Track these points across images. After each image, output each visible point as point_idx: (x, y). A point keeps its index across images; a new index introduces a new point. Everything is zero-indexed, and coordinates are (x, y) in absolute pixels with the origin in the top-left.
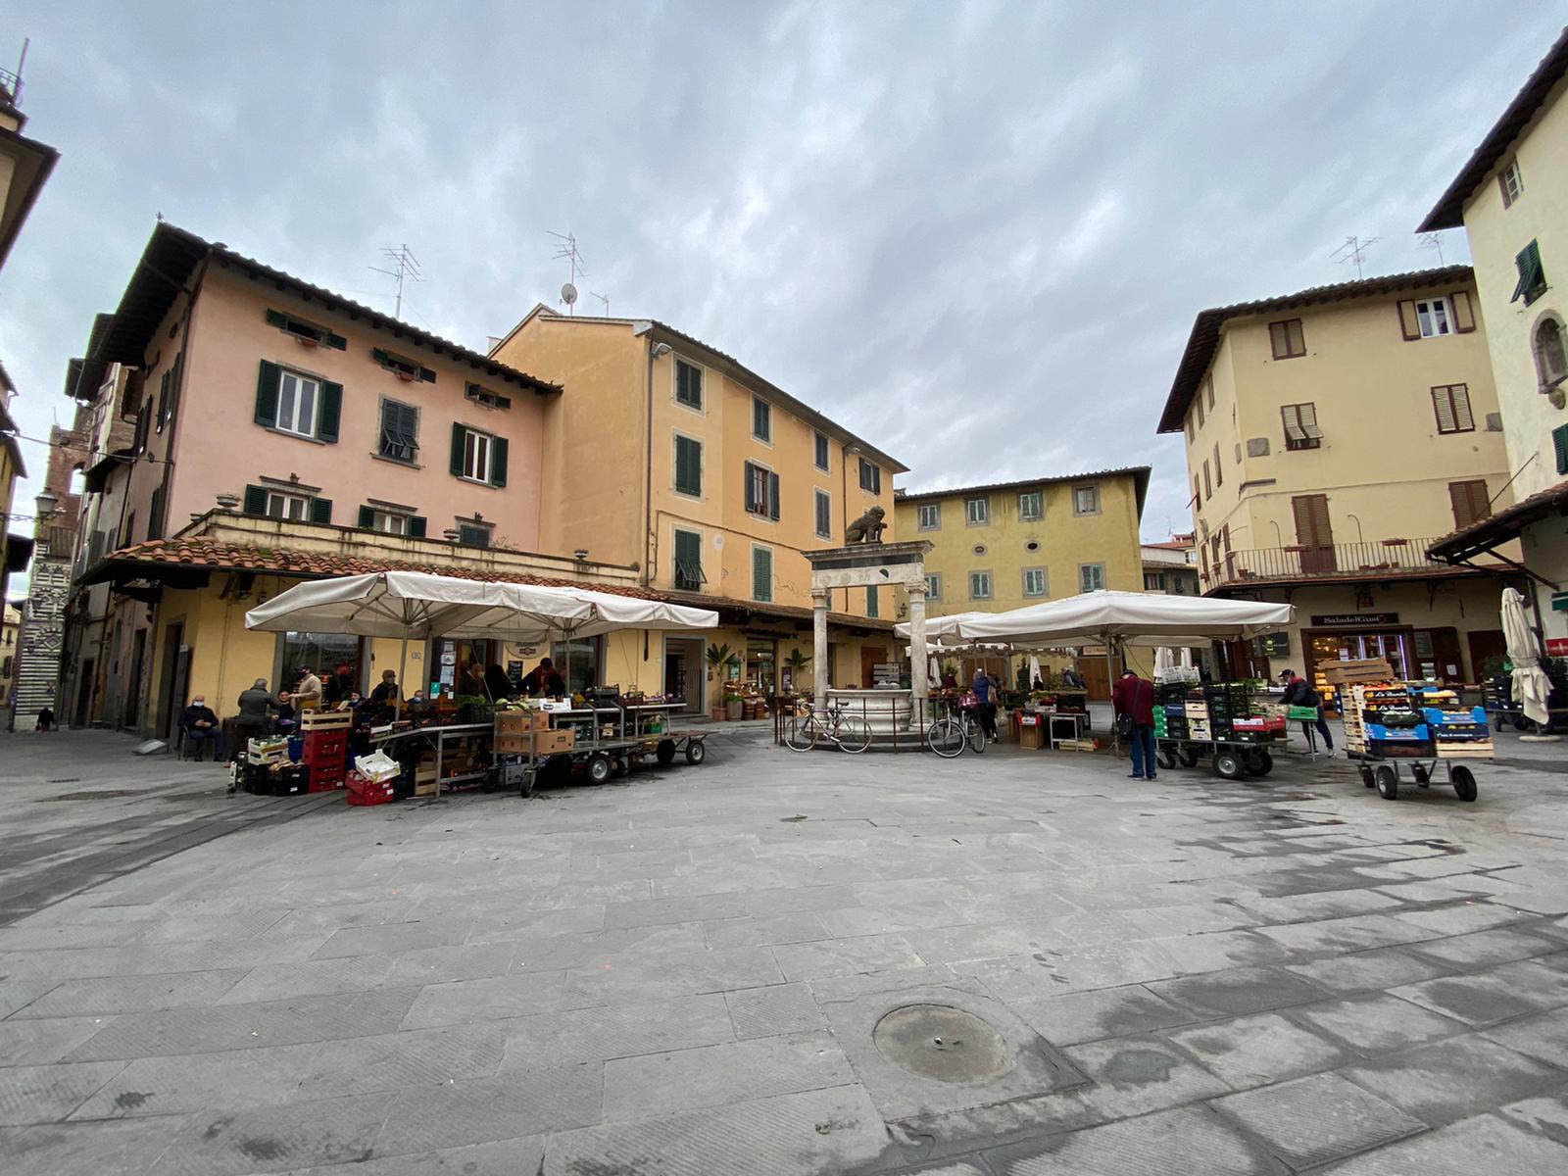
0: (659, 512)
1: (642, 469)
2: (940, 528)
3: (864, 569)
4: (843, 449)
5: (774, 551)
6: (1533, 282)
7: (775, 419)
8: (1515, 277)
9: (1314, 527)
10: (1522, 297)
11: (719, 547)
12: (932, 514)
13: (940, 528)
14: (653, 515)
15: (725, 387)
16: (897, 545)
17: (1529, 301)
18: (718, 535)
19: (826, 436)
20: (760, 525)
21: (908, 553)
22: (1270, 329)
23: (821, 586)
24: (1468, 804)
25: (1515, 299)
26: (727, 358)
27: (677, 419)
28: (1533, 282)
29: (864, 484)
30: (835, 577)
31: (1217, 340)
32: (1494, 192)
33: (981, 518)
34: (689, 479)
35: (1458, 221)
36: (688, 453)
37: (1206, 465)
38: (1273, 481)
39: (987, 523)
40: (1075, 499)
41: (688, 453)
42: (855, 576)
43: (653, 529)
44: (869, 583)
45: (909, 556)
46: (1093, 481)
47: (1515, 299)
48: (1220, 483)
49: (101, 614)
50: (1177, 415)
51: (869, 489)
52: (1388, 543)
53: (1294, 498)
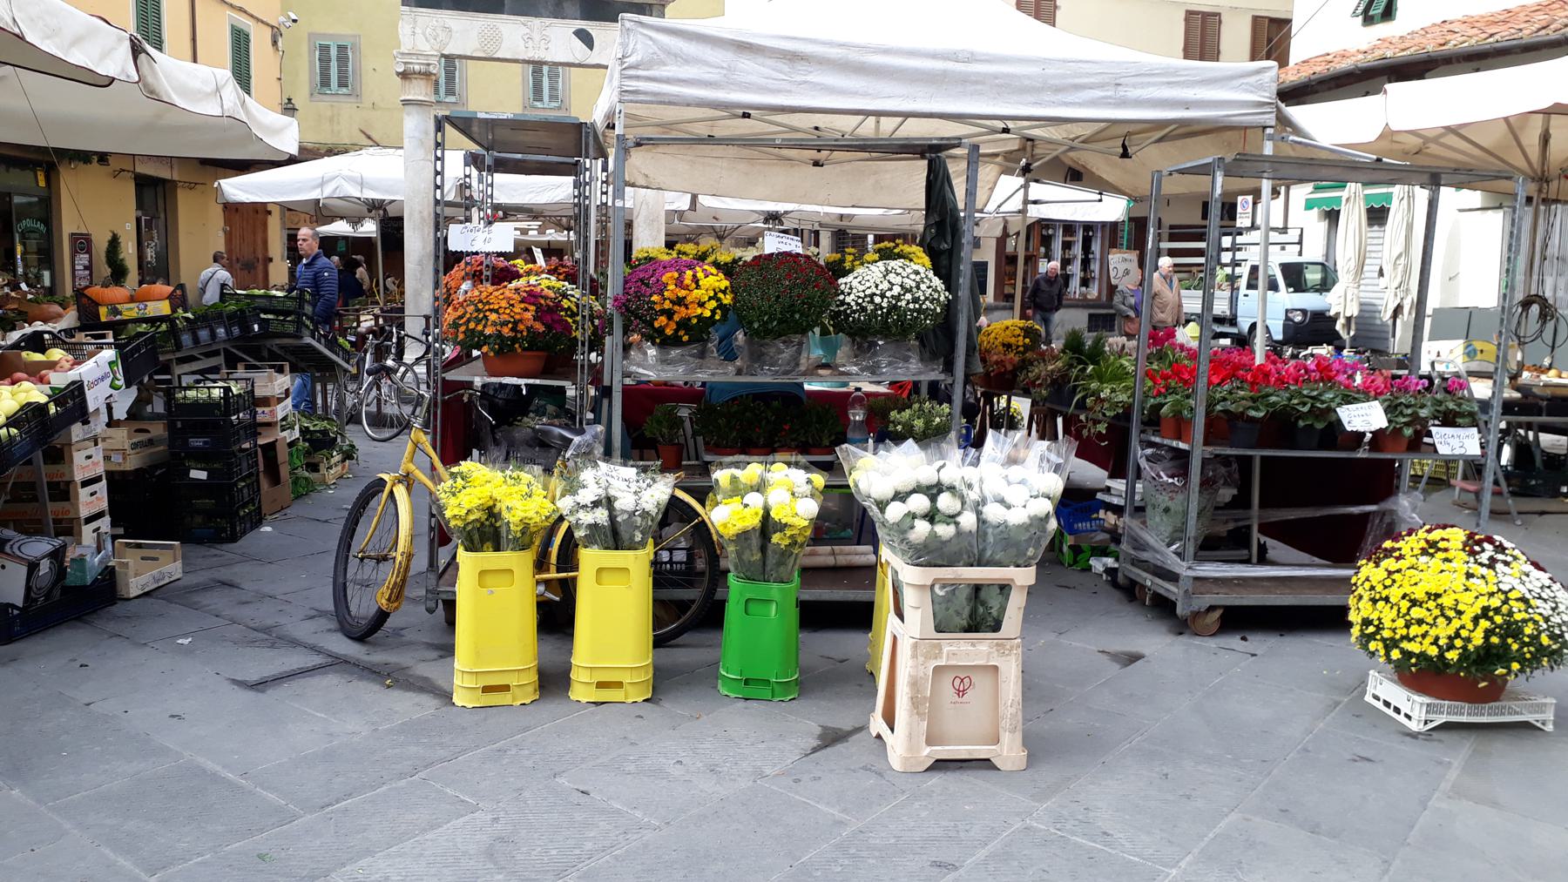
3: (536, 22)
23: (425, 47)
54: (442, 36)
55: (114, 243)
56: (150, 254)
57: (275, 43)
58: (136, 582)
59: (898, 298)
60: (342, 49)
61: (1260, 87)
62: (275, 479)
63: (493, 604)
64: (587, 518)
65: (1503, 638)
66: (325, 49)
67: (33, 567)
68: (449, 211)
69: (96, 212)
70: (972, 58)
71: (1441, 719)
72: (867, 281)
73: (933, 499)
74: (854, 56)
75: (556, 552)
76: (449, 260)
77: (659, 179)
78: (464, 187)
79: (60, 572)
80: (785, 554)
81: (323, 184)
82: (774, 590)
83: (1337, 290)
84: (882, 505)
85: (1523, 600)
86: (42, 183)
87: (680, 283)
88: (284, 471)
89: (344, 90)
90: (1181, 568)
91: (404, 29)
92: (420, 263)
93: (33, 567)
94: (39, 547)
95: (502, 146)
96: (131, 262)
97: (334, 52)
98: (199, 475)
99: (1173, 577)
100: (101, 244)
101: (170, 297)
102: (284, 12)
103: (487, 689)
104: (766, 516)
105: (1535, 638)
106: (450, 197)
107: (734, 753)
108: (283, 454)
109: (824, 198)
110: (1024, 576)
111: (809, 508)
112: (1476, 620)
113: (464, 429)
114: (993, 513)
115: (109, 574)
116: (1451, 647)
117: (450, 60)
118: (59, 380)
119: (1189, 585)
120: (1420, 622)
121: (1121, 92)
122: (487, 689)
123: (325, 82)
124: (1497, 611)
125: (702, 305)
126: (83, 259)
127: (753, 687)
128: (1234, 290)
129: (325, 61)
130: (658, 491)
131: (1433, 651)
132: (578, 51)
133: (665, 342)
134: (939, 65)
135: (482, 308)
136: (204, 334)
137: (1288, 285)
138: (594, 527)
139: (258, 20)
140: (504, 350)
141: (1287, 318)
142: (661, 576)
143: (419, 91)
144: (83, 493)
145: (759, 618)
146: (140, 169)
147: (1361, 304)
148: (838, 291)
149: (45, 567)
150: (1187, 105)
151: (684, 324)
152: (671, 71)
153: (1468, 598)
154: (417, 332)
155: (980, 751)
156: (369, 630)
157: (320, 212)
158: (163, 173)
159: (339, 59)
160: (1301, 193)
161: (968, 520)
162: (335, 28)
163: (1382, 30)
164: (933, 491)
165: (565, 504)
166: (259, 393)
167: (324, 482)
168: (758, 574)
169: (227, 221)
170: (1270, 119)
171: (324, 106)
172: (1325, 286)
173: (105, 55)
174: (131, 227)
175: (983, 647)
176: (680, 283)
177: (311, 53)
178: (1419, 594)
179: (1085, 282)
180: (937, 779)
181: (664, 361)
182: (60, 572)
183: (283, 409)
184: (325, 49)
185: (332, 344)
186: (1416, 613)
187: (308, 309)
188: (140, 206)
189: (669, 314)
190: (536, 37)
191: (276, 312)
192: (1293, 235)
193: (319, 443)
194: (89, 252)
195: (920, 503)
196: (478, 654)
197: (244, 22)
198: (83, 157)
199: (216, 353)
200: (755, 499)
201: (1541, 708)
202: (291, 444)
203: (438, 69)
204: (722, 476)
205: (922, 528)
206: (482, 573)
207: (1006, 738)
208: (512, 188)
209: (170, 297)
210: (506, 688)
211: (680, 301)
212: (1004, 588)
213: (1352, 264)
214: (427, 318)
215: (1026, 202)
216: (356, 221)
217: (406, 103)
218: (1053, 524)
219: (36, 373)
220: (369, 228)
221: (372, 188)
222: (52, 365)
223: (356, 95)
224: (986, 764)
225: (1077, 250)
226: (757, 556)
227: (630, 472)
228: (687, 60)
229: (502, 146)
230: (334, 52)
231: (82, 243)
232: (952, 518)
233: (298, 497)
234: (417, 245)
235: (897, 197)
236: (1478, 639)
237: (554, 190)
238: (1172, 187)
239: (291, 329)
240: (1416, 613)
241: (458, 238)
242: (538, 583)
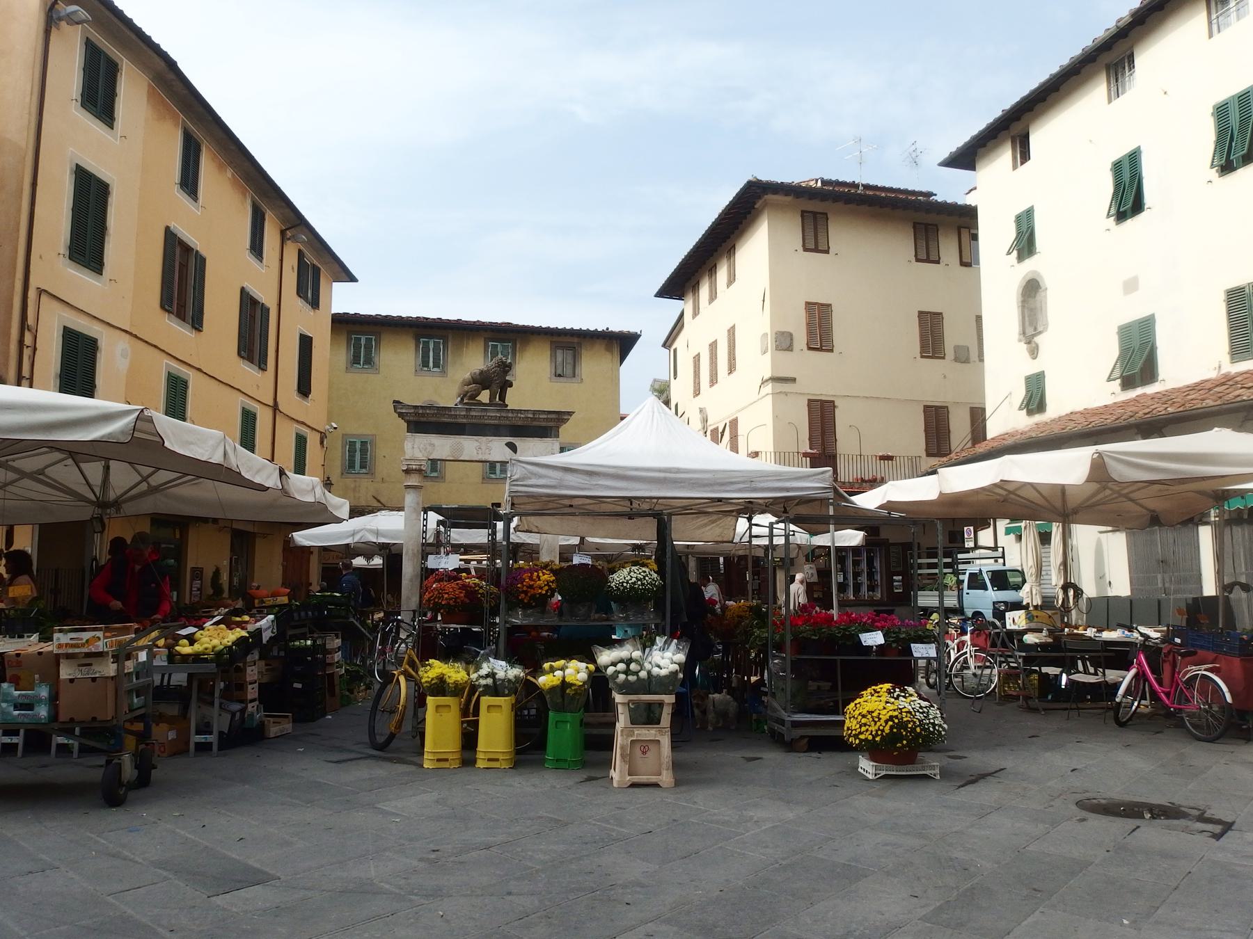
0: (41, 292)
1: (19, 210)
2: (377, 371)
3: (484, 439)
4: (283, 233)
5: (193, 378)
6: (1025, 244)
7: (209, 170)
8: (1012, 235)
9: (823, 433)
10: (1015, 252)
11: (122, 365)
12: (368, 348)
13: (377, 371)
14: (32, 294)
15: (151, 94)
16: (535, 412)
17: (1020, 258)
18: (124, 343)
19: (264, 207)
20: (173, 331)
21: (544, 424)
22: (802, 216)
23: (420, 455)
24: (469, 769)
25: (1009, 253)
26: (164, 56)
27: (76, 139)
28: (1025, 244)
29: (301, 292)
30: (441, 446)
31: (750, 213)
32: (1005, 156)
33: (436, 365)
34: (88, 246)
35: (971, 167)
36: (91, 195)
37: (713, 346)
38: (794, 380)
39: (444, 372)
40: (553, 357)
41: (91, 195)
42: (471, 447)
43: (31, 320)
44: (491, 459)
45: (545, 428)
46: (576, 340)
47: (1009, 253)
48: (732, 368)
49: (153, 484)
50: (682, 283)
51: (305, 298)
52: (883, 458)
53: (809, 401)
54: (429, 448)
55: (217, 573)
56: (236, 580)
57: (322, 443)
58: (274, 730)
59: (634, 583)
60: (364, 444)
61: (824, 480)
62: (333, 694)
63: (440, 725)
64: (483, 682)
65: (899, 730)
66: (352, 444)
67: (233, 715)
68: (428, 549)
69: (207, 555)
70: (678, 471)
71: (883, 773)
72: (623, 577)
73: (628, 666)
74: (621, 472)
75: (469, 701)
76: (427, 573)
77: (548, 529)
78: (438, 533)
79: (242, 719)
80: (573, 698)
81: (354, 534)
82: (568, 716)
83: (1026, 587)
84: (606, 667)
85: (909, 712)
86: (178, 536)
87: (531, 578)
88: (337, 689)
90: (784, 715)
91: (408, 446)
92: (411, 580)
93: (233, 715)
94: (236, 707)
95: (457, 517)
96: (226, 587)
97: (358, 446)
98: (298, 686)
99: (782, 722)
100: (208, 574)
101: (288, 595)
102: (329, 421)
103: (439, 760)
104: (564, 681)
105: (913, 730)
106: (431, 541)
107: (545, 789)
108: (337, 681)
109: (607, 539)
110: (669, 699)
111: (583, 676)
112: (886, 722)
113: (429, 647)
114: (656, 671)
115: (262, 724)
116: (877, 735)
117: (434, 462)
118: (251, 628)
119: (788, 725)
120: (865, 725)
121: (754, 485)
122: (439, 760)
123: (352, 465)
124: (896, 717)
125: (541, 588)
126: (197, 583)
127: (561, 765)
128: (960, 590)
129: (352, 451)
130: (515, 672)
131: (870, 737)
132: (506, 454)
133: (525, 607)
134: (662, 475)
135: (441, 591)
136: (303, 614)
137: (993, 586)
138: (486, 686)
139: (313, 429)
140: (451, 613)
141: (995, 608)
142: (517, 709)
143: (414, 480)
144: (250, 687)
145: (563, 731)
146: (234, 526)
147: (1043, 597)
148: (607, 581)
149: (238, 714)
150: (788, 490)
151: (533, 597)
152: (529, 482)
153: (884, 712)
154: (408, 620)
155: (653, 779)
156: (382, 747)
157: (349, 551)
158: (250, 528)
160: (1002, 524)
161: (643, 674)
163: (1038, 418)
164: (628, 661)
165: (474, 676)
166: (328, 647)
167: (356, 699)
168: (561, 709)
169: (285, 559)
170: (831, 495)
171: (349, 481)
172: (1018, 587)
173: (268, 477)
174: (226, 563)
175: (653, 732)
176: (531, 578)
177: (343, 447)
178: (865, 712)
179: (871, 588)
180: (631, 790)
181: (525, 615)
182: (242, 719)
183: (338, 656)
185: (364, 624)
186: (864, 721)
187: (353, 603)
188: (232, 550)
189: (526, 593)
190: (483, 448)
191: (336, 605)
192: (999, 553)
193: (354, 678)
194: (201, 579)
195: (621, 666)
196: (435, 744)
197: (304, 430)
198: (205, 520)
199: (304, 626)
200: (559, 673)
201: (933, 768)
202: (341, 676)
204: (546, 666)
205: (622, 677)
206: (438, 707)
207: (664, 773)
208: (460, 536)
209: (288, 595)
210: (446, 760)
211: (531, 587)
212: (661, 704)
213: (1034, 570)
214: (414, 611)
215: (751, 536)
216: (369, 557)
217: (408, 487)
218: (681, 676)
219: (241, 625)
220: (377, 561)
222: (247, 622)
223: (371, 473)
224: (656, 785)
225: (864, 566)
226: (560, 700)
227: (503, 663)
228: (541, 476)
229: (457, 517)
230: (358, 446)
231: (198, 573)
232: (636, 673)
233: (343, 706)
234: (409, 569)
235: (643, 535)
236: (887, 730)
237: (479, 536)
239: (343, 613)
240: (864, 721)
241: (432, 562)
242: (463, 722)
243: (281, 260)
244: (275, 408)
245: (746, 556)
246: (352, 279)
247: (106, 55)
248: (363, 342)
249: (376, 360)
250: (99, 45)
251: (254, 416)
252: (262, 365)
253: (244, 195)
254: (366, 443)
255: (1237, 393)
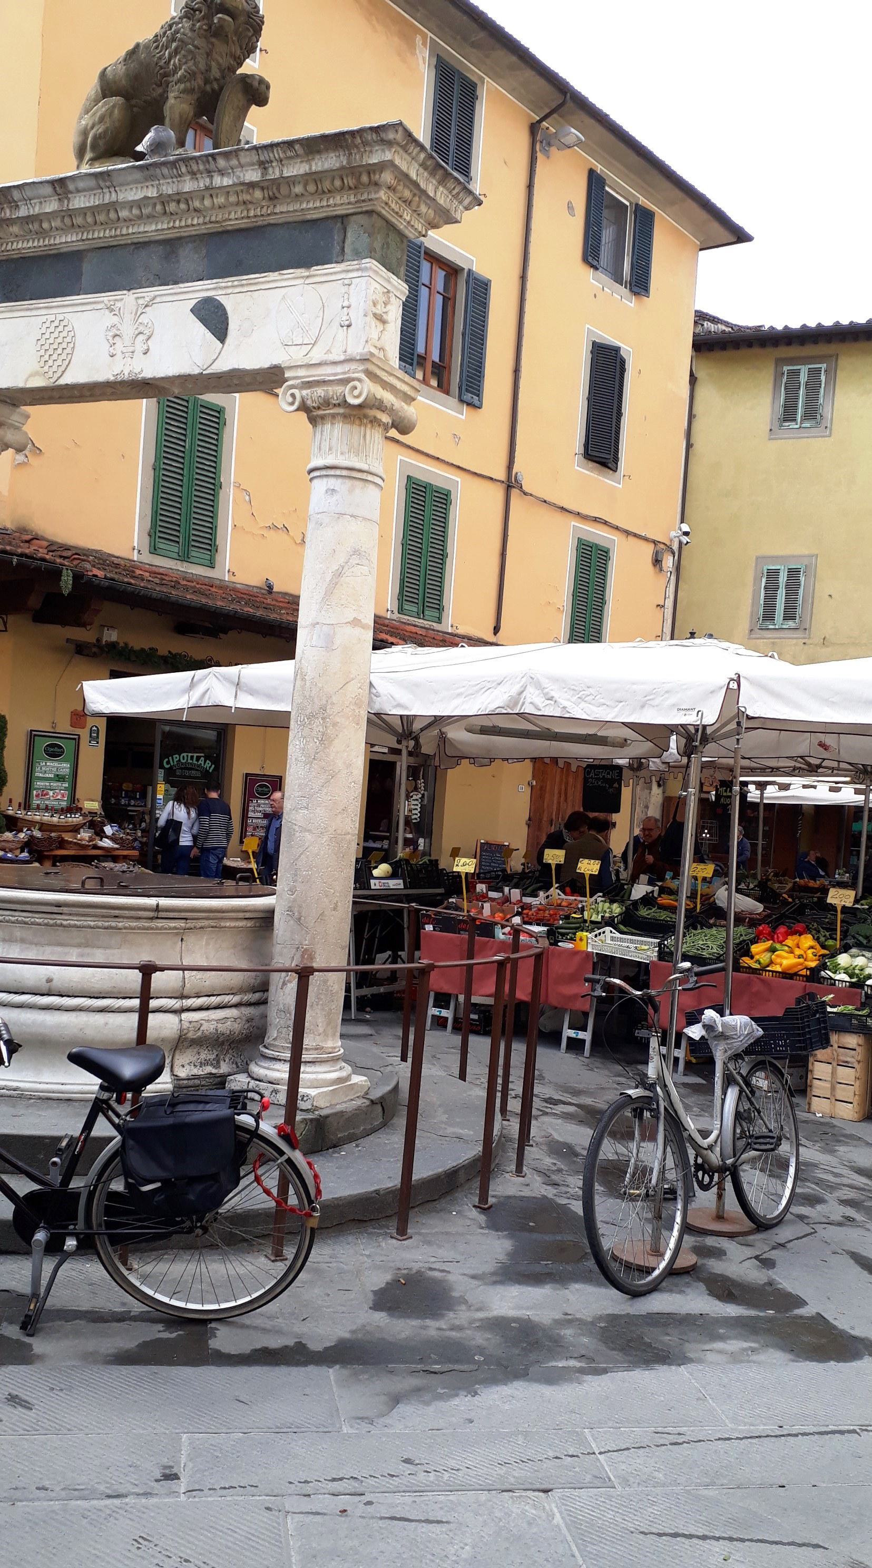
3: (128, 299)
4: (534, 129)
12: (813, 388)
19: (473, 71)
66: (772, 575)
89: (791, 624)
97: (783, 578)
123: (769, 615)
139: (627, 533)
159: (787, 586)
162: (785, 547)
177: (757, 580)
184: (772, 575)
190: (128, 330)
203: (675, 547)
221: (252, 692)
223: (803, 629)
230: (783, 578)
238: (521, 1389)
243: (530, 187)
244: (511, 484)
245: (643, 1139)
246: (740, 236)
247: (460, 74)
248: (803, 378)
249: (826, 411)
250: (452, 62)
251: (443, 499)
252: (470, 390)
253: (407, 36)
254: (797, 571)
255: (849, 1059)
